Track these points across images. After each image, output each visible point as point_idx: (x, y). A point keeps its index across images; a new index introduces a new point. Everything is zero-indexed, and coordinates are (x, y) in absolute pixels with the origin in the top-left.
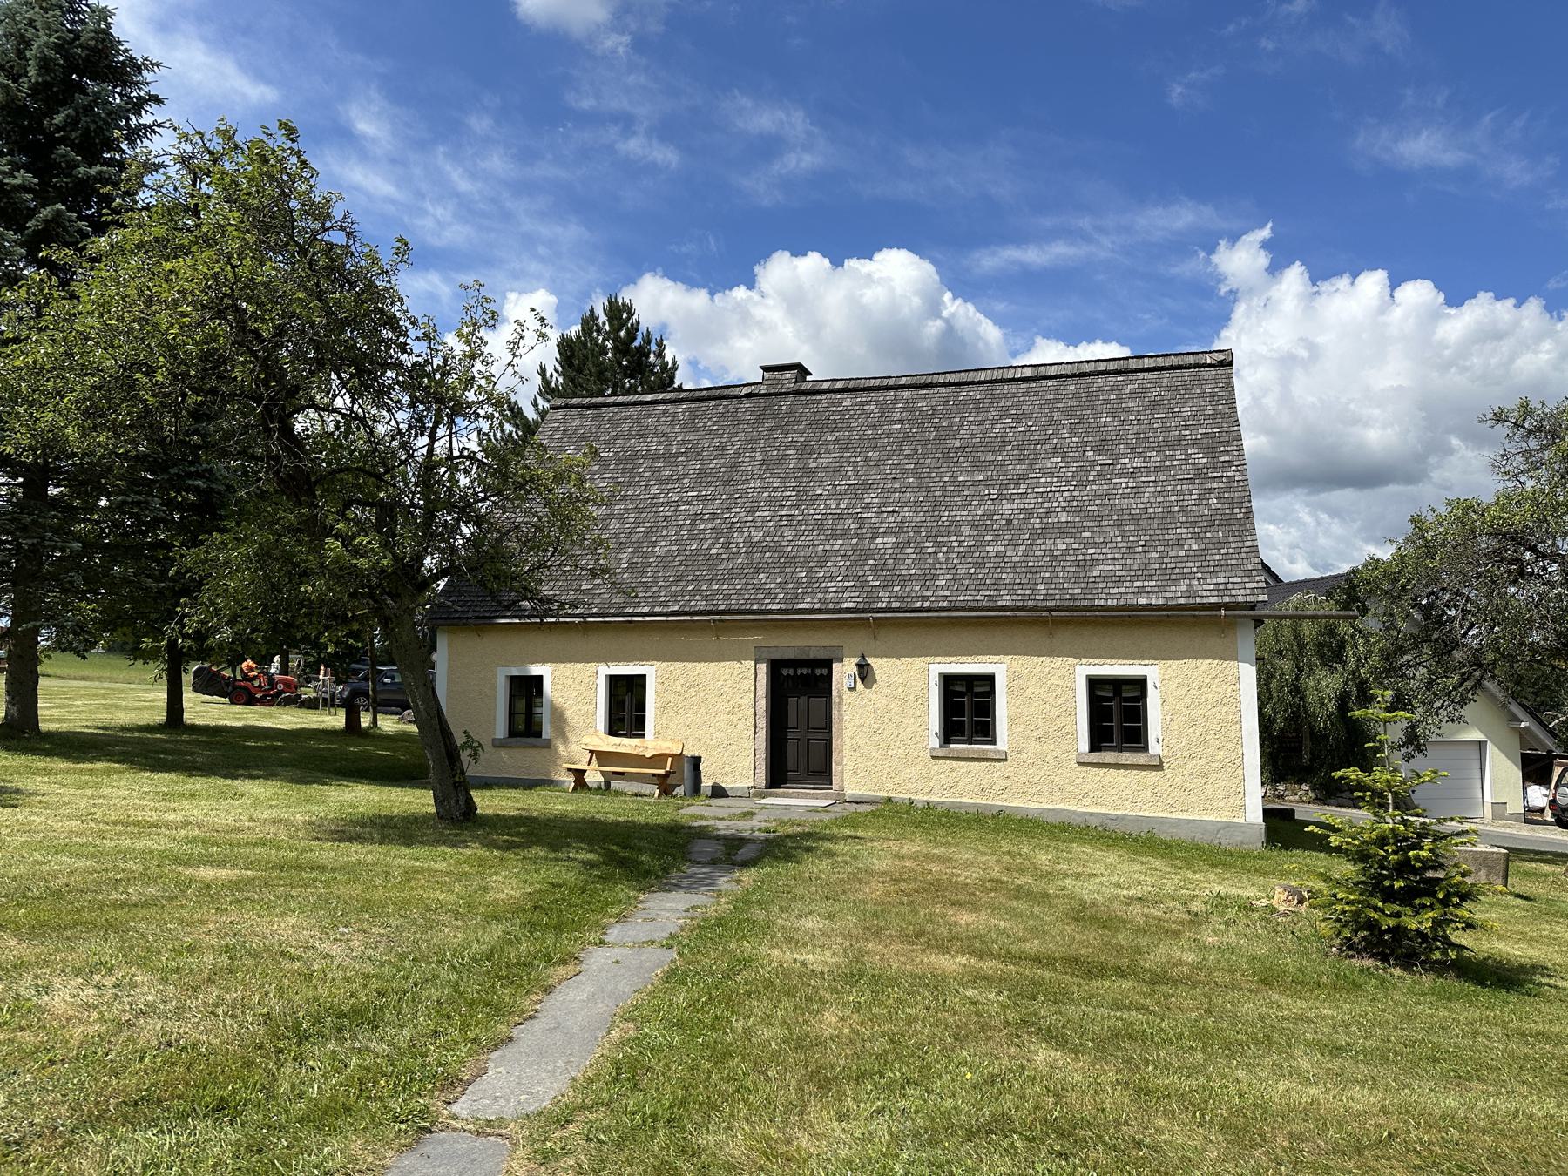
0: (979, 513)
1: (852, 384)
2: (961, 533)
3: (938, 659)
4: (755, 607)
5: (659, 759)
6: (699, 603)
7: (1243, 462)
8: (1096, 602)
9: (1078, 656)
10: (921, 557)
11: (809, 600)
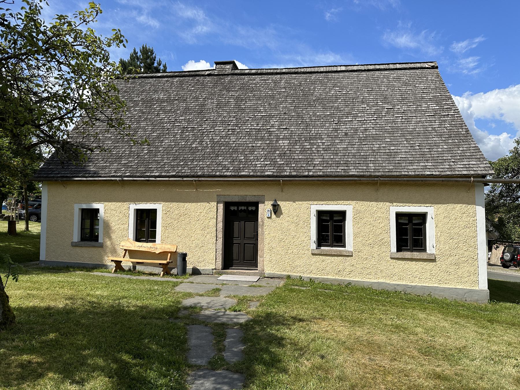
0: (330, 129)
1: (259, 71)
2: (322, 139)
3: (315, 202)
4: (218, 174)
5: (163, 255)
6: (187, 171)
7: (457, 108)
8: (403, 173)
9: (391, 202)
10: (303, 151)
11: (247, 170)
